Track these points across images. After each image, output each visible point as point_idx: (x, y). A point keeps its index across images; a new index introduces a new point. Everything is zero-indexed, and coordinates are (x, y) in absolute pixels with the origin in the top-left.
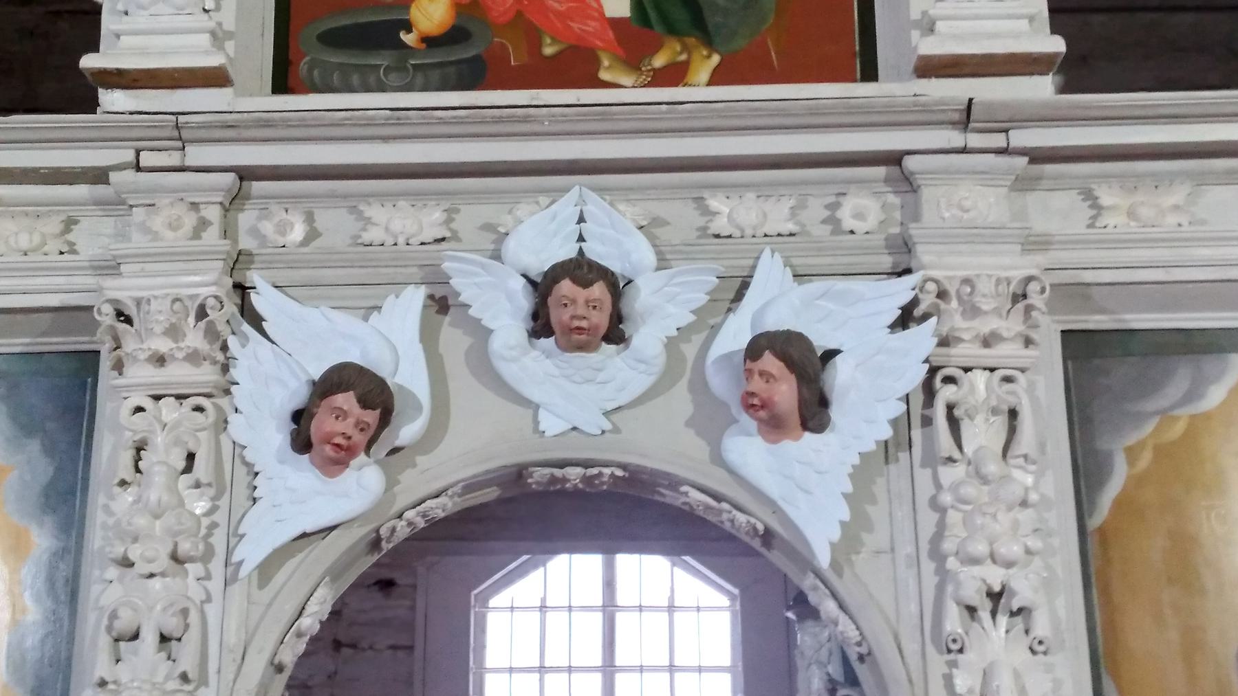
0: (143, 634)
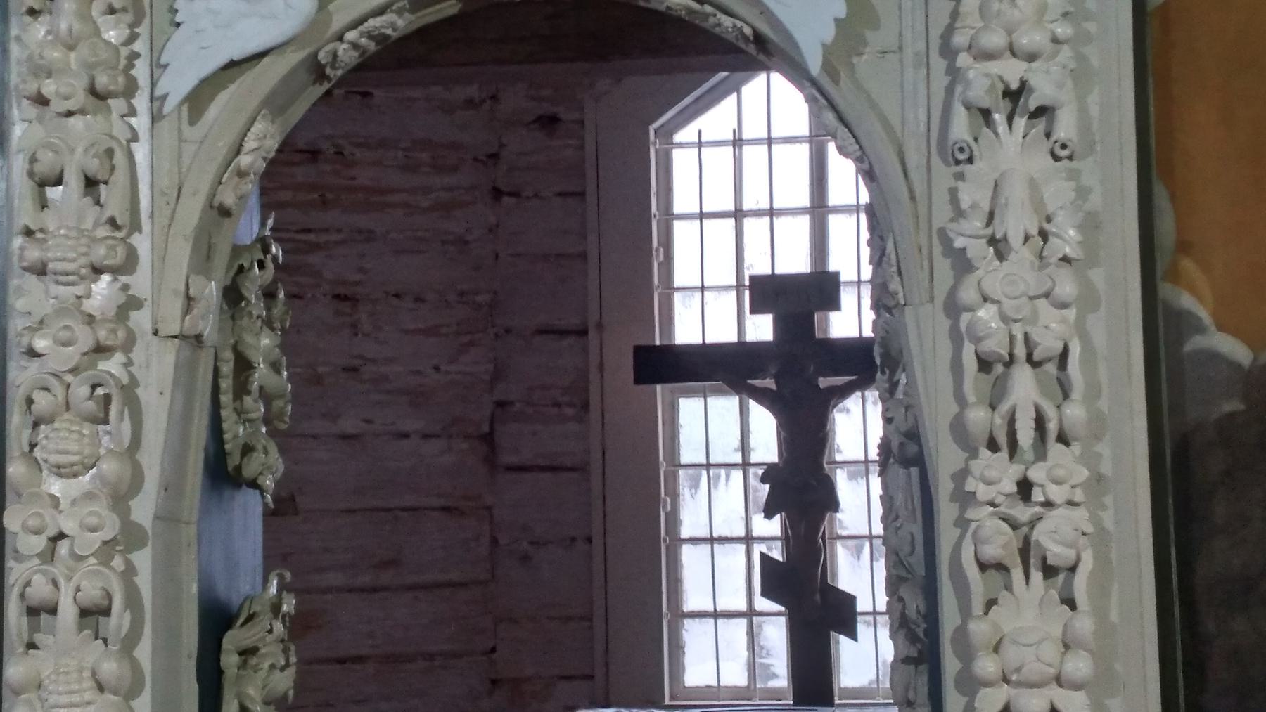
0: (66, 177)
